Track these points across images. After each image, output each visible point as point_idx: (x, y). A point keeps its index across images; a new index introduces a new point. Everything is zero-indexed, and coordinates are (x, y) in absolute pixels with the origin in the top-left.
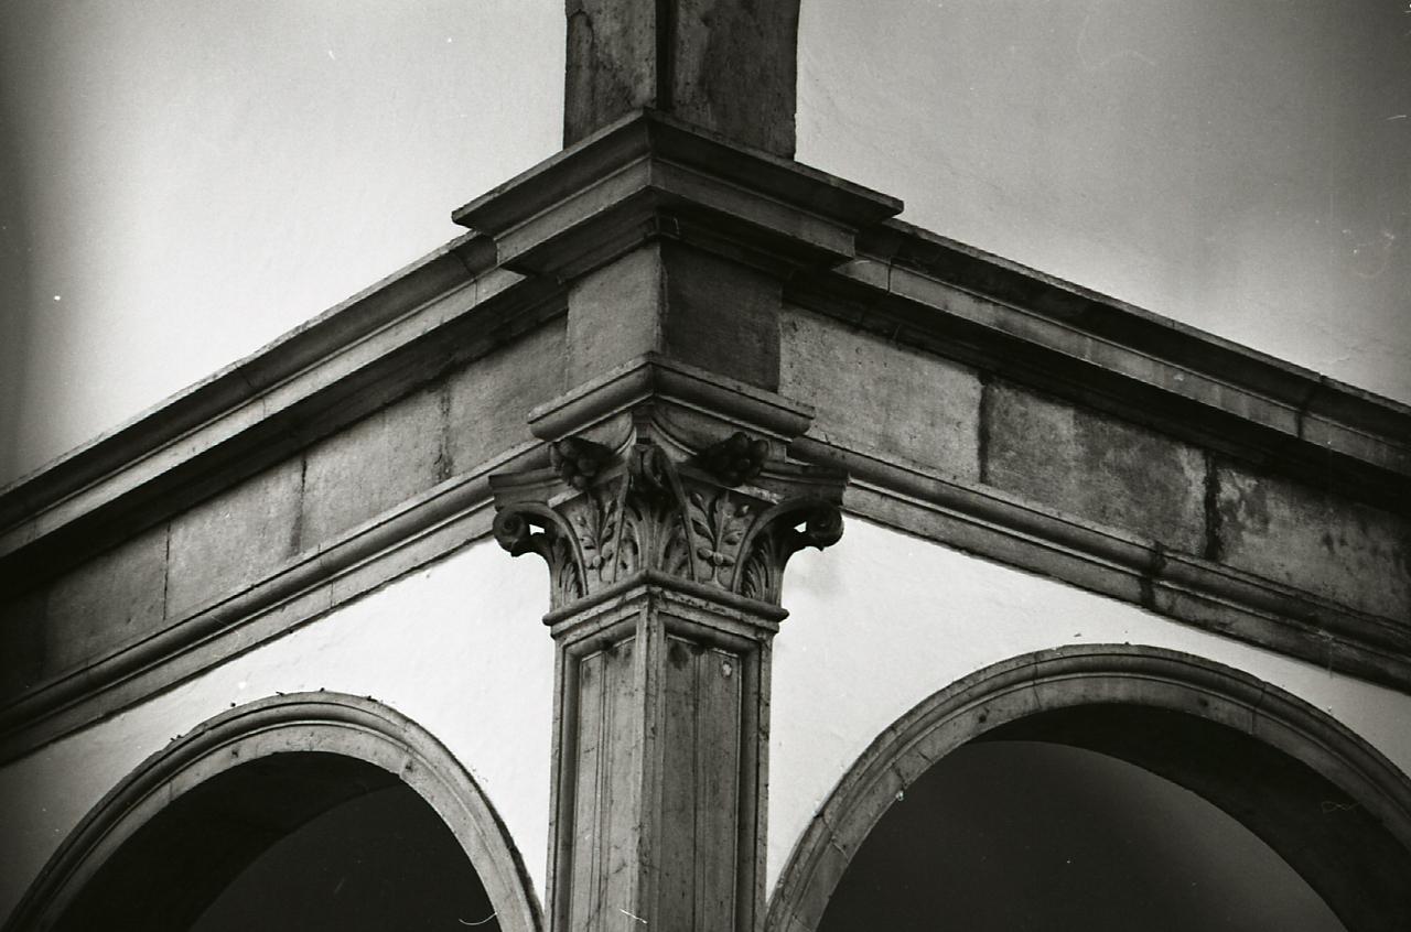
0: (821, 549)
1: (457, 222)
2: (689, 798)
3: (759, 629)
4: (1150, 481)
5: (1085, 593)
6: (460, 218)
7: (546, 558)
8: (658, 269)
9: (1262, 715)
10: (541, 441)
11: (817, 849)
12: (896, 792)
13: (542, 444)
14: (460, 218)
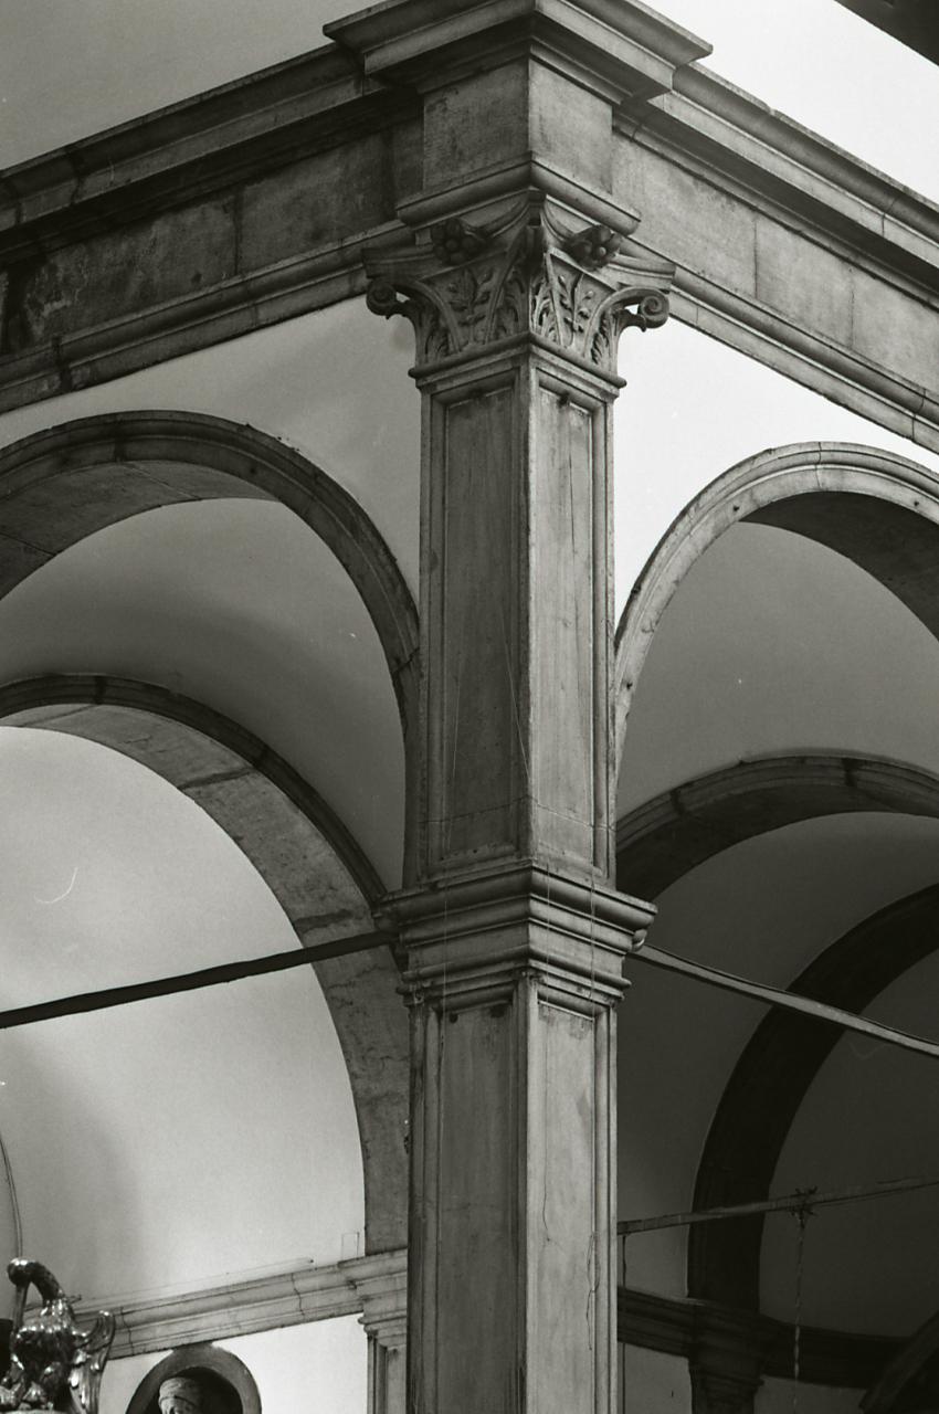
0: (644, 330)
1: (326, 35)
2: (199, 792)
3: (604, 393)
4: (347, 167)
5: (638, 574)
6: (327, 30)
7: (413, 322)
8: (666, 171)
9: (889, 220)
10: (402, 224)
11: (764, 468)
12: (106, 1310)
13: (402, 227)
14: (327, 30)
